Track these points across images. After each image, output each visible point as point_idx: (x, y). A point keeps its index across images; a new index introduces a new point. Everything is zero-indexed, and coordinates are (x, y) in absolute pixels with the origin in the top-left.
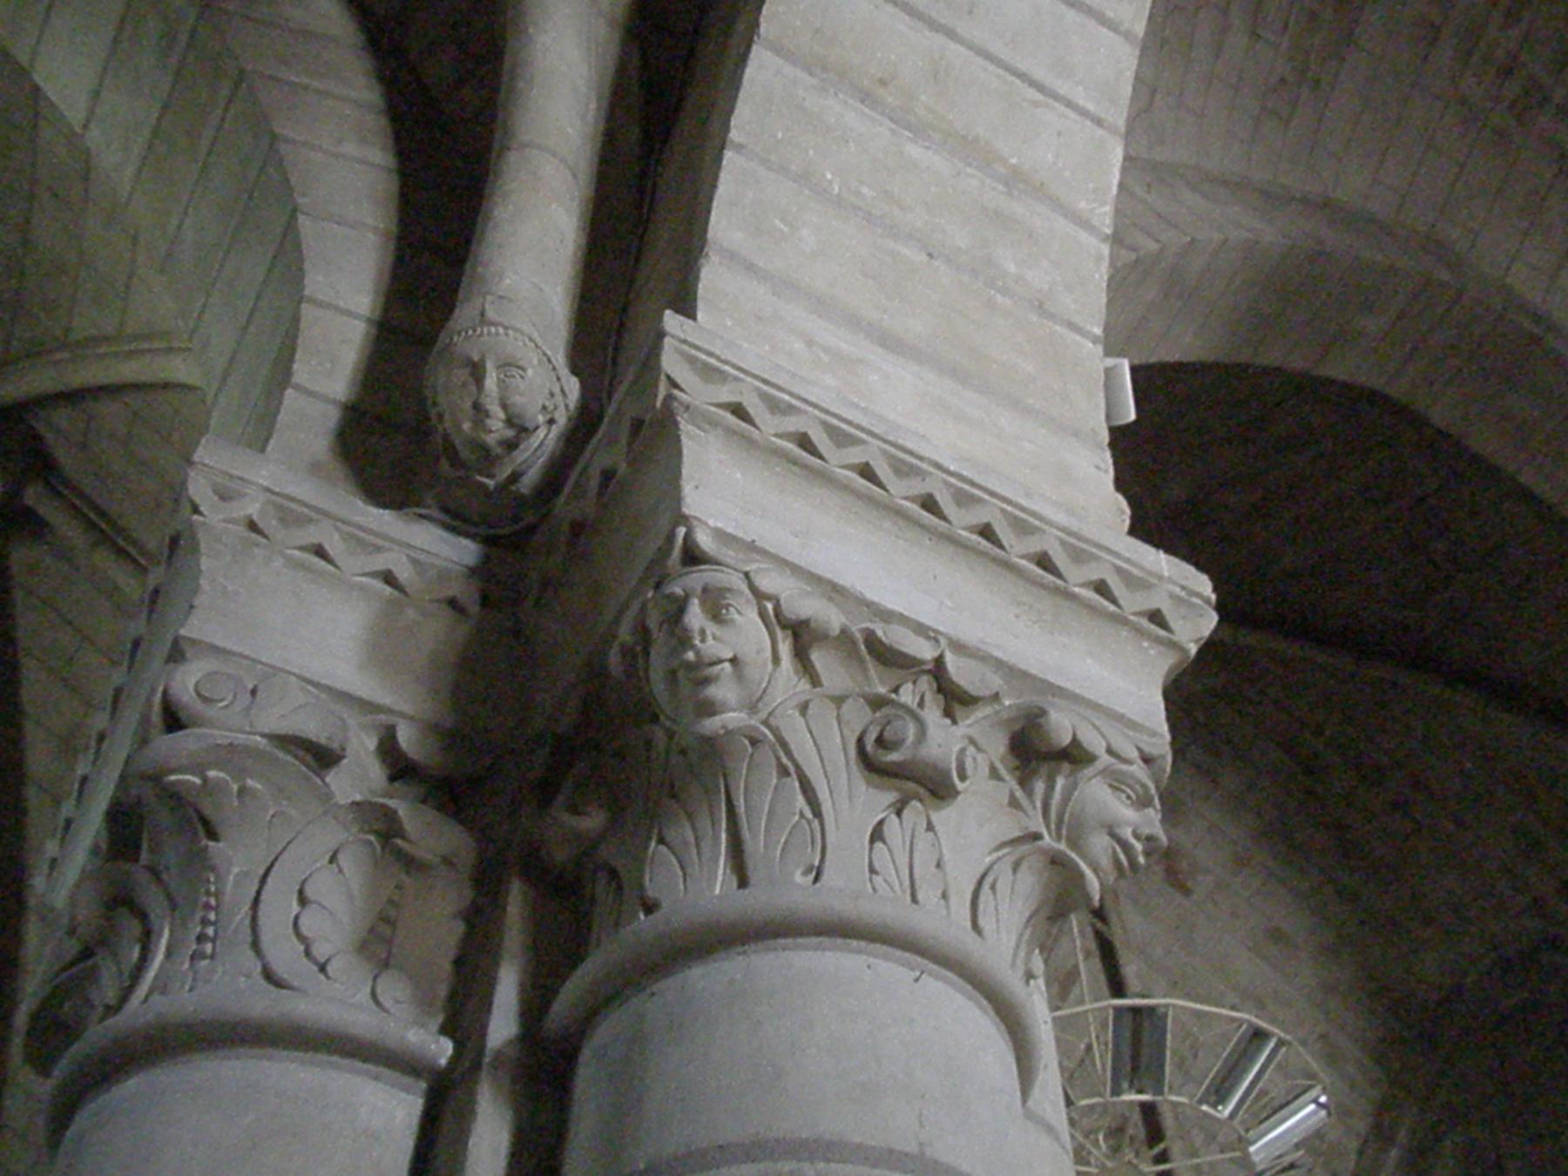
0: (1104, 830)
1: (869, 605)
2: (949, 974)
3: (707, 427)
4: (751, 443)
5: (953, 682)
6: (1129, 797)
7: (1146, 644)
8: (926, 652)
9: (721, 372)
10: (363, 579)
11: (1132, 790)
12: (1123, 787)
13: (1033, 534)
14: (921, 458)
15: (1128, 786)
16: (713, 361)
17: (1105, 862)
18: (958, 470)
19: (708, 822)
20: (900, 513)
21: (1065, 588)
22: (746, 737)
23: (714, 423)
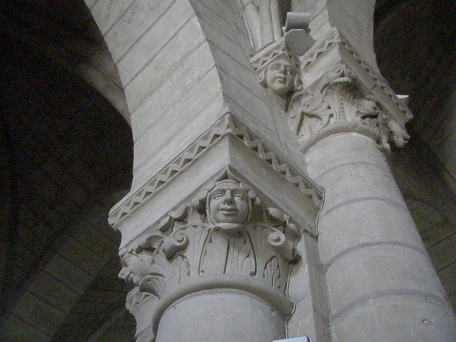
0: (218, 211)
1: (154, 224)
2: (186, 296)
3: (122, 224)
4: (169, 184)
5: (182, 216)
6: (219, 196)
7: (219, 145)
8: (167, 220)
9: (118, 211)
10: (144, 300)
11: (218, 194)
12: (216, 196)
13: (181, 159)
14: (129, 199)
15: (216, 194)
16: (115, 212)
17: (224, 218)
18: (163, 167)
19: (297, 242)
20: (146, 202)
21: (193, 161)
22: (146, 282)
23: (122, 222)
